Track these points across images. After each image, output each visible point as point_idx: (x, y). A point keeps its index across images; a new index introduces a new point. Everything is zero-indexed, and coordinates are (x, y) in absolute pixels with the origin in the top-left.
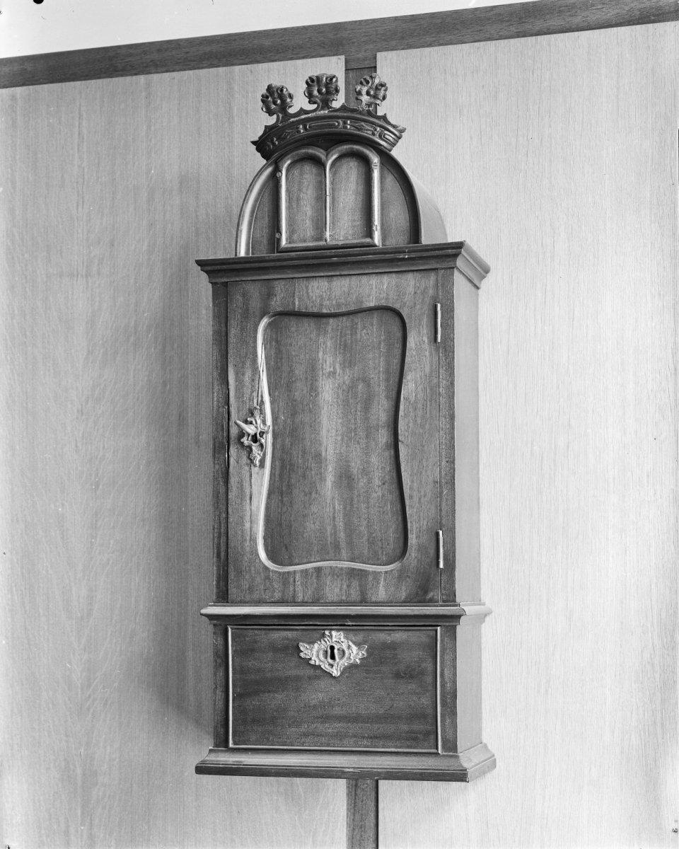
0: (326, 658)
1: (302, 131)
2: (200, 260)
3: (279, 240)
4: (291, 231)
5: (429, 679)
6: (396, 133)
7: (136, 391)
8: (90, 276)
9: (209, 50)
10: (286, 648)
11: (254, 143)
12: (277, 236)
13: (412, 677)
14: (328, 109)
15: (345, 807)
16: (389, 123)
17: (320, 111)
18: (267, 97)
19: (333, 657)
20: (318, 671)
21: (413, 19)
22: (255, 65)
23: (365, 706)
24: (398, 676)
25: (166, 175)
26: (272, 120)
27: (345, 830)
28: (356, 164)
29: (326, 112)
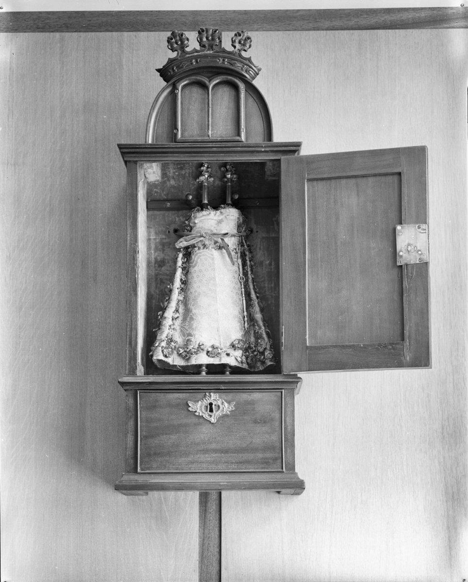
0: (207, 411)
1: (194, 63)
2: (122, 145)
3: (176, 135)
4: (182, 134)
5: (277, 424)
6: (256, 71)
7: (51, 244)
8: (17, 164)
9: (105, 20)
10: (178, 405)
11: (158, 70)
12: (175, 131)
13: (265, 422)
14: (213, 50)
15: (198, 525)
16: (254, 65)
17: (207, 51)
18: (172, 39)
19: (211, 410)
20: (201, 420)
21: (246, 12)
22: (139, 33)
23: (232, 442)
24: (255, 422)
25: (74, 100)
26: (174, 55)
27: (198, 541)
28: (228, 89)
29: (211, 52)
